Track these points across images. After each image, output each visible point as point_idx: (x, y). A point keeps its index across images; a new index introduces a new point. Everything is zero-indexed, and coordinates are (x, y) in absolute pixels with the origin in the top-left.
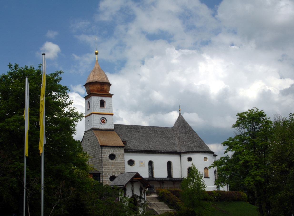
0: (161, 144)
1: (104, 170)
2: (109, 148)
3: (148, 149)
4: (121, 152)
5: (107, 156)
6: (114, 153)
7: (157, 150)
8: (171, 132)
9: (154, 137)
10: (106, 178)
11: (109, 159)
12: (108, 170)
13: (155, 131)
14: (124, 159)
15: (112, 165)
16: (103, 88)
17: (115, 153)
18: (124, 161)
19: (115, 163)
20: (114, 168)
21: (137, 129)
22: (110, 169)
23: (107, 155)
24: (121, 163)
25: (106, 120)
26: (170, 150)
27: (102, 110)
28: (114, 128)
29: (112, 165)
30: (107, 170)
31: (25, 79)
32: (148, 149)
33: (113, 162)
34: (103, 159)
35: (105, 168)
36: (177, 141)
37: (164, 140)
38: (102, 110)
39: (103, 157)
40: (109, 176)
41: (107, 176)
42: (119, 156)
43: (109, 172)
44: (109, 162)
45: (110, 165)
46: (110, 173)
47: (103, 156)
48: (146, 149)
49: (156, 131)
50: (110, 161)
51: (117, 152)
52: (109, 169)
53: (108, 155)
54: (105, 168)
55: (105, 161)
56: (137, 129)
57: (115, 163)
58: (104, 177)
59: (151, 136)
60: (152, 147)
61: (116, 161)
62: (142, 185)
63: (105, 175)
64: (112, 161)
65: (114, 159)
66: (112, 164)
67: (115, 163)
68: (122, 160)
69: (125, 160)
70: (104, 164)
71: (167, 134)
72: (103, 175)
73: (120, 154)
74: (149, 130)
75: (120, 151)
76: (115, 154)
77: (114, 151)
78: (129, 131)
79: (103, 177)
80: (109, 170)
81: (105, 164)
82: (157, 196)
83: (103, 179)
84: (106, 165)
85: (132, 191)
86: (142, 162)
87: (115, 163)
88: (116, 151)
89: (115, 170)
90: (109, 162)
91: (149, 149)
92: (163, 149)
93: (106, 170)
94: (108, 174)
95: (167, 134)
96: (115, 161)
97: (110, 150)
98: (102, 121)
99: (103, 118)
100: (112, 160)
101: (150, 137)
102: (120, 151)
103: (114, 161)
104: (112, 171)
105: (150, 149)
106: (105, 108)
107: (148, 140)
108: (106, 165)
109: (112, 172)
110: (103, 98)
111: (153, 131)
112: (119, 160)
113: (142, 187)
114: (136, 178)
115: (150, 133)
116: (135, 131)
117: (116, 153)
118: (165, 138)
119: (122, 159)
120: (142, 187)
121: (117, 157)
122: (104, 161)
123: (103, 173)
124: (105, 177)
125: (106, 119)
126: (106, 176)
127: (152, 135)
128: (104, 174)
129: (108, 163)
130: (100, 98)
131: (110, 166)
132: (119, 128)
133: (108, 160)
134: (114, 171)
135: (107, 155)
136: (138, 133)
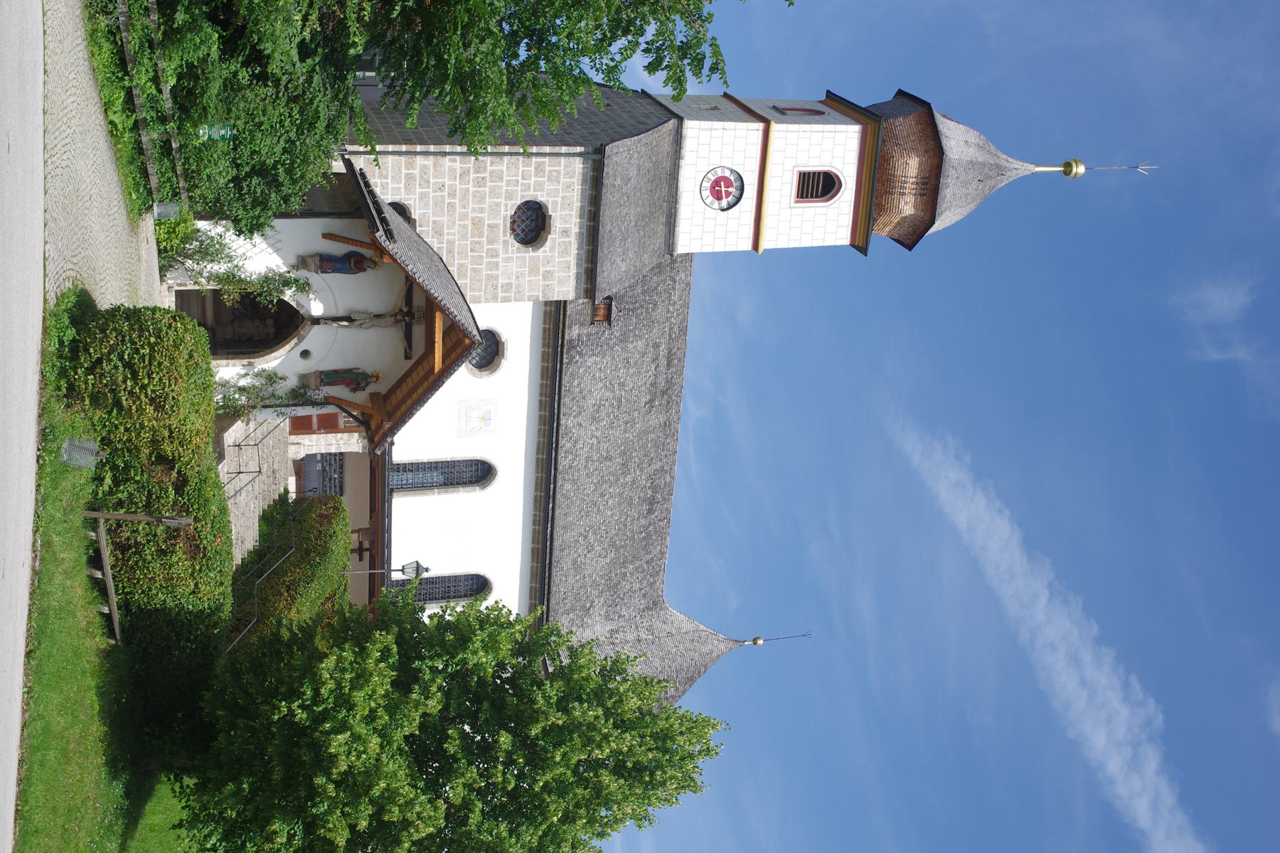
0: (586, 537)
1: (452, 170)
2: (586, 204)
3: (562, 455)
4: (561, 282)
5: (539, 186)
6: (554, 238)
7: (557, 512)
8: (644, 596)
9: (620, 495)
10: (396, 179)
11: (519, 202)
12: (452, 195)
13: (652, 502)
14: (516, 300)
15: (477, 223)
16: (904, 194)
17: (554, 240)
18: (506, 300)
19: (491, 241)
20: (464, 237)
21: (664, 393)
22: (454, 211)
23: (542, 190)
24: (489, 278)
25: (724, 203)
26: (554, 589)
27: (782, 184)
28: (681, 255)
29: (477, 223)
30: (450, 186)
31: (581, 145)
32: (561, 454)
33: (496, 226)
34: (521, 158)
35: (465, 173)
36: (598, 628)
37: (605, 557)
38: (782, 184)
39: (529, 165)
40: (411, 202)
41: (409, 188)
42: (534, 270)
43: (438, 203)
44: (498, 205)
45: (482, 210)
46: (427, 204)
47: (534, 159)
48: (562, 442)
49: (650, 511)
50: (508, 209)
51: (562, 253)
52: (457, 201)
53: (541, 198)
54: (465, 173)
55: (505, 178)
56: (664, 393)
57: (491, 241)
58: (407, 168)
59: (629, 479)
60: (574, 482)
61: (507, 252)
62: (382, 387)
63: (417, 172)
64: (505, 219)
65: (517, 237)
66: (487, 222)
67: (491, 241)
68: (507, 287)
69: (513, 304)
70: (485, 170)
71: (632, 574)
72: (420, 160)
73: (547, 275)
74: (659, 465)
75: (562, 274)
76: (548, 243)
77: (565, 232)
78: (656, 346)
79: (403, 159)
80: (447, 201)
81: (487, 175)
82: (290, 501)
83: (396, 157)
84: (480, 183)
85: (341, 313)
86: (485, 419)
87: (491, 241)
88: (565, 252)
89: (451, 243)
90: (498, 205)
91: (563, 462)
92: (562, 550)
93: (447, 183)
94: (423, 196)
95: (632, 574)
96: (505, 242)
97: (574, 213)
98: (717, 183)
99: (742, 189)
100: (509, 221)
101: (625, 474)
102: (562, 274)
103: (505, 235)
104: (444, 219)
105: (560, 468)
106: (796, 202)
107: (609, 458)
108: (480, 183)
109: (434, 222)
110: (846, 198)
111: (650, 492)
112: (514, 267)
113: (367, 384)
114: (446, 334)
115: (641, 470)
116: (654, 385)
117: (552, 249)
118: (613, 563)
119: (518, 286)
120: (372, 388)
121: (529, 253)
122: (505, 168)
123: (430, 161)
124: (404, 172)
125: (730, 207)
126: (410, 177)
127: (633, 482)
128: (424, 169)
129: (494, 192)
130: (848, 173)
131: (474, 210)
132: (674, 288)
133: (509, 196)
134: (446, 231)
135: (542, 190)
136: (644, 400)
